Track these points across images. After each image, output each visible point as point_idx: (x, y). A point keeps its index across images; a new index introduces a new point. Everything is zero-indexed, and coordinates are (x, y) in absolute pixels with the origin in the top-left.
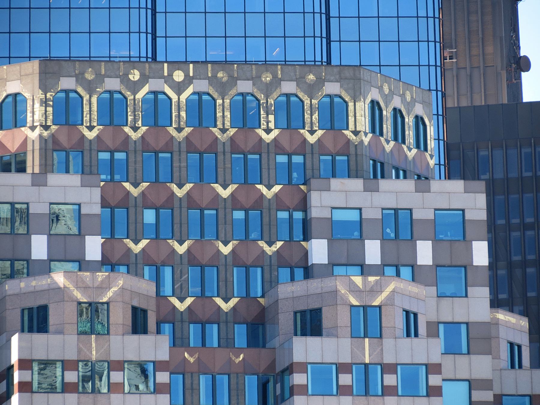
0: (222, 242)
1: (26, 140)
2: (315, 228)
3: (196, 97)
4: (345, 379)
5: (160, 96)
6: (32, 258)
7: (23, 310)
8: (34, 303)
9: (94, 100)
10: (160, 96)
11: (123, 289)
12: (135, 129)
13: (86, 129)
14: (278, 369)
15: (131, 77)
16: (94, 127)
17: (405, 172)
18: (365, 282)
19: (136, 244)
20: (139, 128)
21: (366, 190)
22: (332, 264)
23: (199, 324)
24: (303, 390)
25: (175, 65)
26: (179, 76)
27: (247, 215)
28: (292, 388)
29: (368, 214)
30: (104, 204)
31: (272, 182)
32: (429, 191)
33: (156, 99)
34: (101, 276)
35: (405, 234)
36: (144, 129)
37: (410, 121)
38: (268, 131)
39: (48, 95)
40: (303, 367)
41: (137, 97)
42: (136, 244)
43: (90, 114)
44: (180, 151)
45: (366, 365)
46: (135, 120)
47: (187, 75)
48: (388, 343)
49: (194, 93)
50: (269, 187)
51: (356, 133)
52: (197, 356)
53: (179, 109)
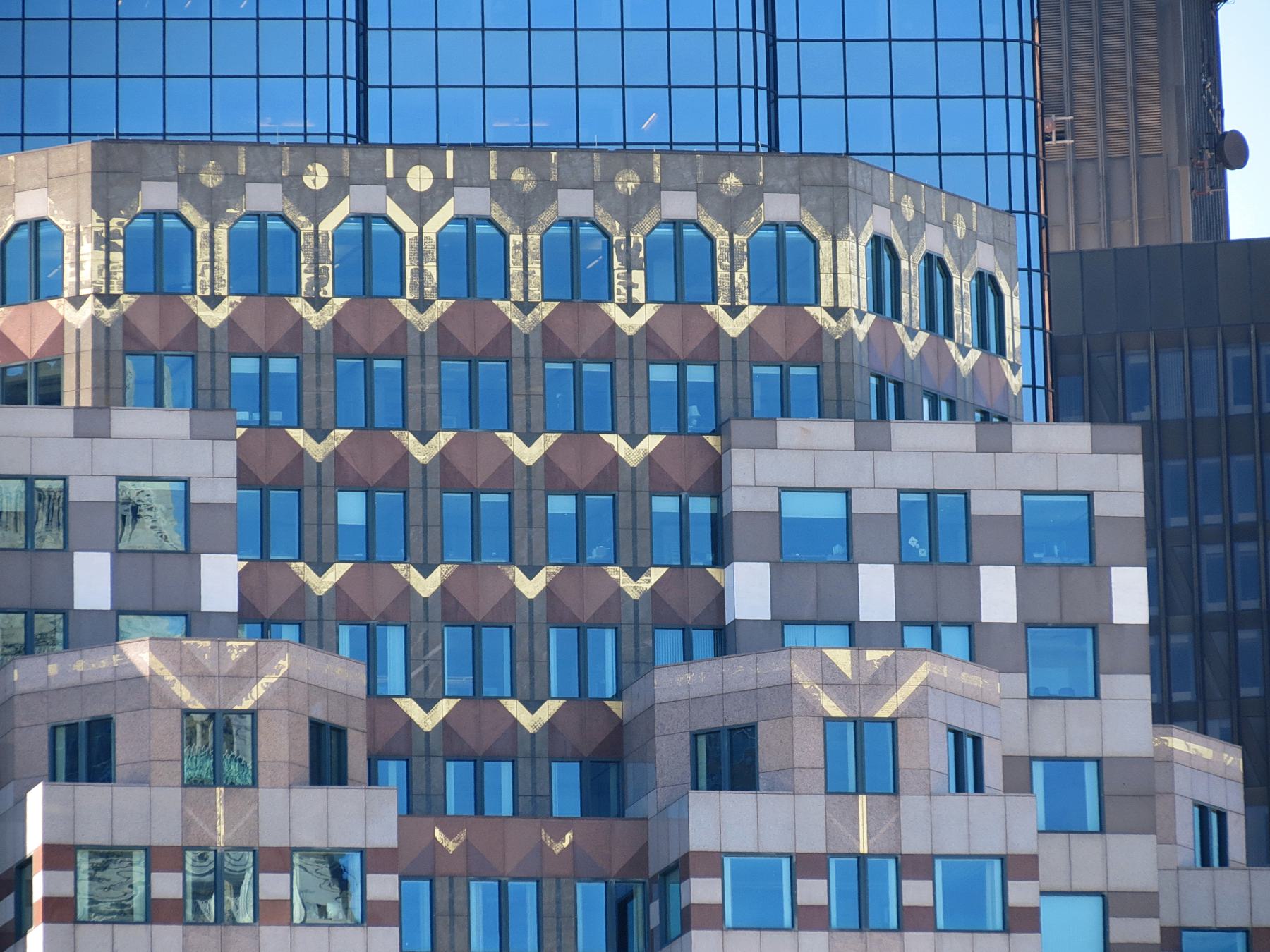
0: (522, 569)
1: (60, 329)
2: (740, 536)
3: (461, 228)
4: (812, 891)
5: (377, 227)
6: (76, 607)
7: (54, 730)
8: (81, 713)
9: (222, 234)
10: (377, 227)
11: (288, 679)
12: (318, 303)
13: (201, 304)
14: (655, 867)
15: (307, 180)
16: (221, 298)
17: (952, 403)
18: (857, 664)
19: (320, 574)
20: (327, 300)
21: (860, 446)
22: (782, 621)
23: (467, 761)
24: (713, 917)
25: (411, 152)
27: (580, 505)
28: (686, 913)
29: (865, 504)
30: (246, 479)
31: (639, 428)
32: (1009, 450)
33: (366, 233)
34: (237, 648)
35: (952, 549)
36: (339, 302)
37: (963, 284)
38: (630, 308)
39: (114, 224)
40: (712, 863)
41: (322, 227)
42: (320, 574)
43: (212, 268)
44: (423, 356)
45: (861, 858)
46: (317, 283)
47: (439, 177)
48: (912, 805)
49: (456, 219)
50: (633, 440)
51: (837, 312)
52: (462, 836)
53: (421, 257)
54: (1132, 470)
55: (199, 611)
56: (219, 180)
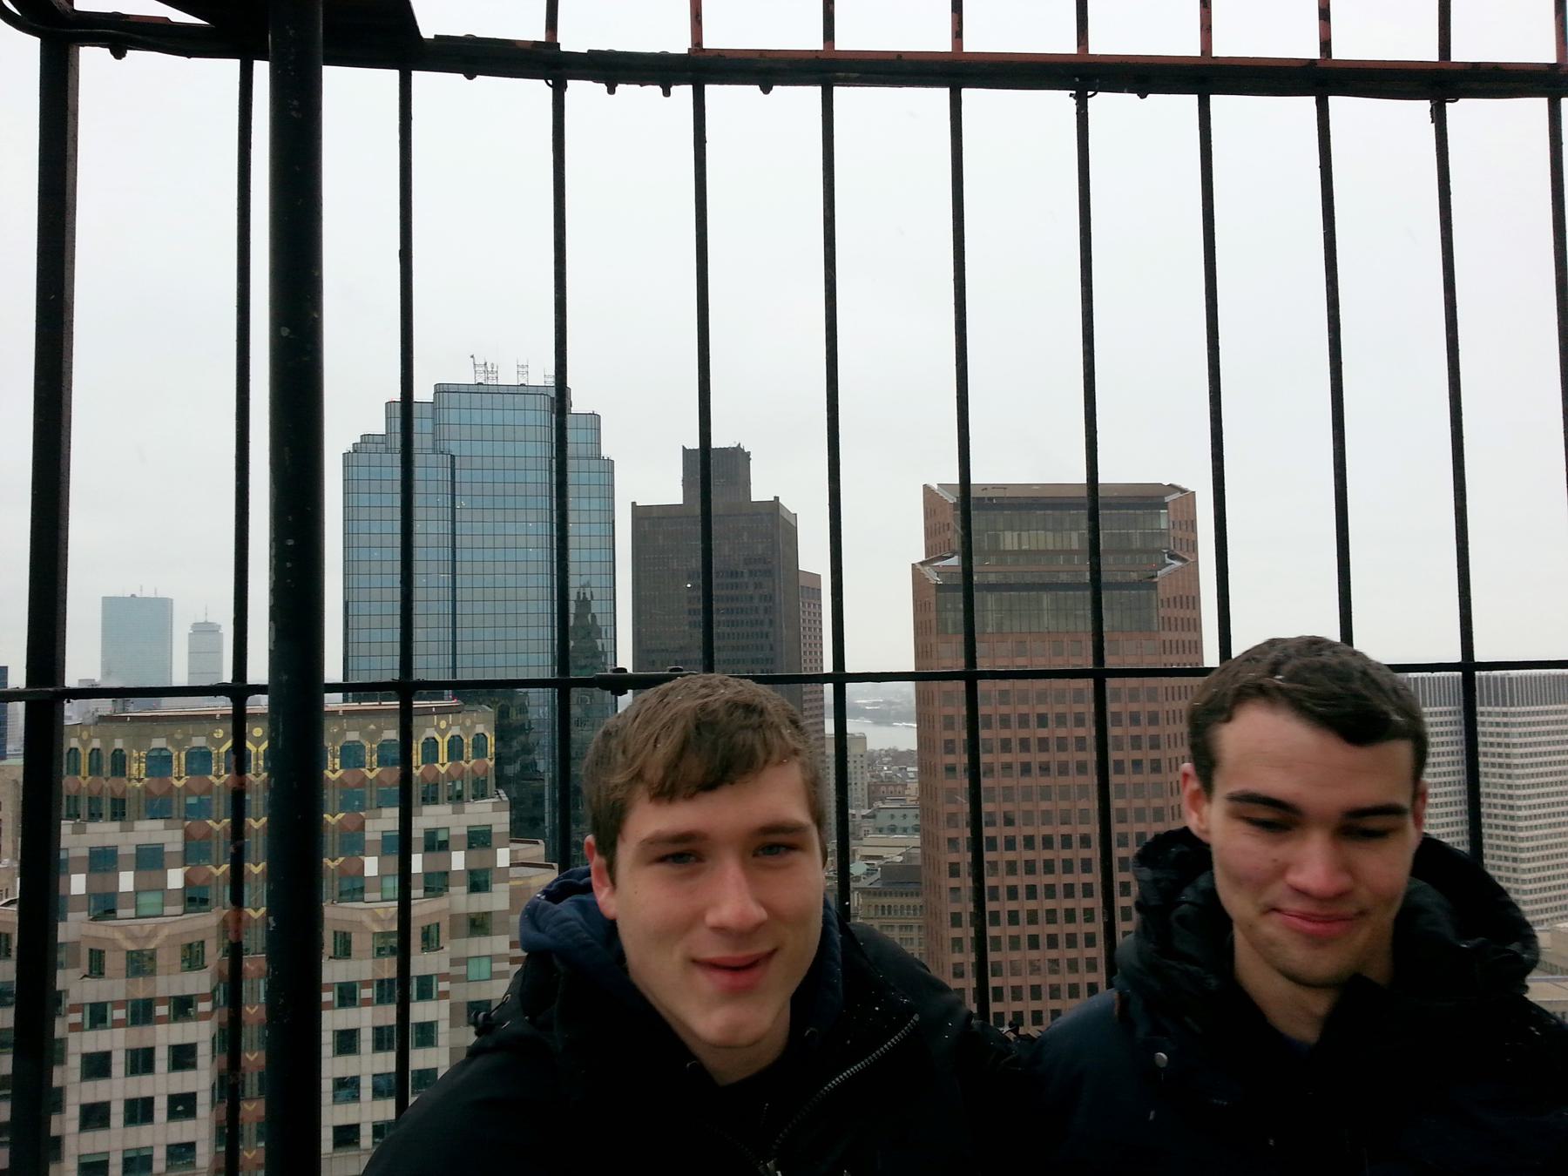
0: (254, 864)
1: (463, 771)
6: (72, 893)
9: (183, 756)
12: (218, 777)
13: (175, 780)
15: (215, 735)
16: (182, 777)
19: (218, 869)
20: (222, 776)
26: (443, 724)
32: (464, 813)
38: (334, 771)
39: (142, 754)
41: (259, 749)
42: (218, 869)
43: (179, 767)
46: (218, 770)
47: (448, 724)
53: (257, 760)
54: (505, 817)
55: (379, 856)
56: (220, 730)
